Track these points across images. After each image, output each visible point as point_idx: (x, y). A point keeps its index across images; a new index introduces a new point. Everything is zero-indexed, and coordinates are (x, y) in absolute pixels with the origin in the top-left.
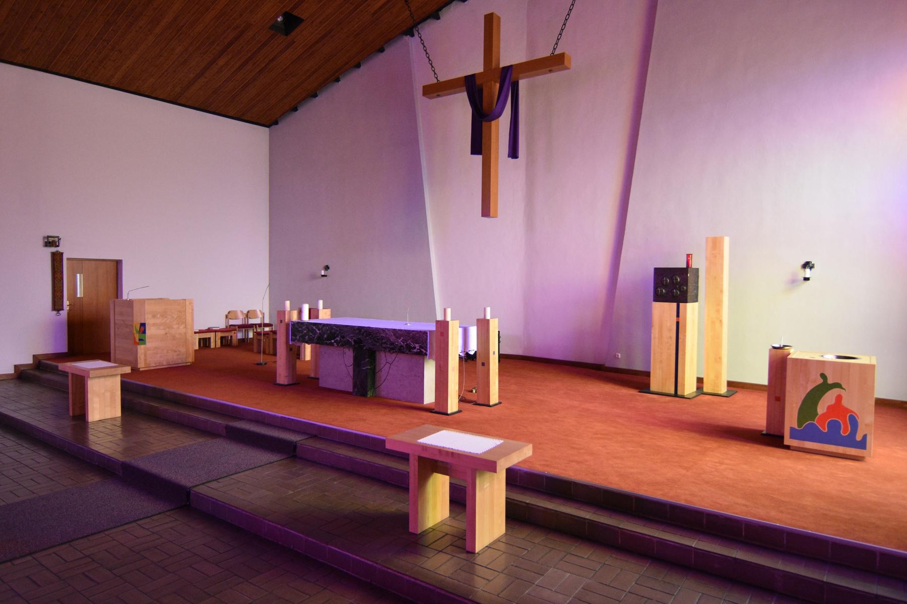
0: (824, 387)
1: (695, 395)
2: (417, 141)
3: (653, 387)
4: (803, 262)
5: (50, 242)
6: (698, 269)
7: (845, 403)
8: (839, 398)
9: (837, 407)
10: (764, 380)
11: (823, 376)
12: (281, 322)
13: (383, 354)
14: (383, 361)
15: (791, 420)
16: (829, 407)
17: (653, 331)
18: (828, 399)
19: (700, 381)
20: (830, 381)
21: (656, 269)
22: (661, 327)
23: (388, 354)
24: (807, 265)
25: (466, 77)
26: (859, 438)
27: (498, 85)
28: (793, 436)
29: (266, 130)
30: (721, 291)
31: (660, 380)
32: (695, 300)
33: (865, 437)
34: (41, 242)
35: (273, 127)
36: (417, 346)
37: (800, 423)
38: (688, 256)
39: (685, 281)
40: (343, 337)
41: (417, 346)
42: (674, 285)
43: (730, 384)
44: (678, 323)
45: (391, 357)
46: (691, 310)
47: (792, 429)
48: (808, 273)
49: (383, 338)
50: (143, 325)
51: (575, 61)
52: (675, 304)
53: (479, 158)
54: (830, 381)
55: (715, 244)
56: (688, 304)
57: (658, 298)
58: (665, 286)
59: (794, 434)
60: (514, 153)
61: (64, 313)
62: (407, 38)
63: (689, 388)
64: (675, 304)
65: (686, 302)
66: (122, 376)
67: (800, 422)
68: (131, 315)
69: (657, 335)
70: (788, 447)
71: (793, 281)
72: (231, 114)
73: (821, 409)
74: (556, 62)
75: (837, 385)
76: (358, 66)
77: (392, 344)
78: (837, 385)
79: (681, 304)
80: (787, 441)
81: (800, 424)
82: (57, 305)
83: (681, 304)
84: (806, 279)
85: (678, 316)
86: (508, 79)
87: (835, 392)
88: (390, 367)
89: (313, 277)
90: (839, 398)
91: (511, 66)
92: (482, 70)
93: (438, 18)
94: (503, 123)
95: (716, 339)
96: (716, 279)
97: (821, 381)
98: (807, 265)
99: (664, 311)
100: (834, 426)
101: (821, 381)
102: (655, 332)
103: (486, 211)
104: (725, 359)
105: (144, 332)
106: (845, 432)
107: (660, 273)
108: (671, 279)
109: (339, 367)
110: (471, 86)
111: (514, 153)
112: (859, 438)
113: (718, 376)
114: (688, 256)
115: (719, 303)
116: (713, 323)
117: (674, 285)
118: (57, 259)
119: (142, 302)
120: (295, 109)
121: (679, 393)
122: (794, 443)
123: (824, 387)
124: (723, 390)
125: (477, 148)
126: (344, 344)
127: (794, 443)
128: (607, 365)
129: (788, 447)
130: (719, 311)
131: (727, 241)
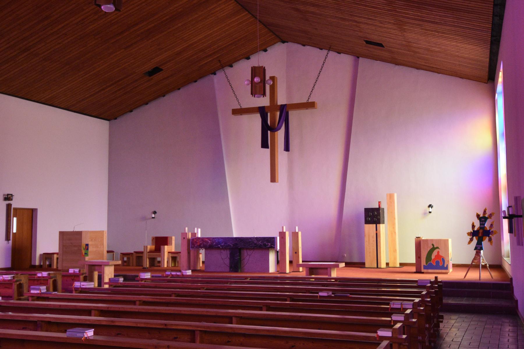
0: (434, 249)
2: (220, 135)
5: (8, 198)
7: (440, 254)
8: (438, 252)
9: (438, 256)
10: (414, 261)
11: (433, 245)
12: (184, 238)
13: (245, 251)
14: (246, 254)
15: (423, 262)
18: (435, 253)
19: (387, 264)
20: (435, 247)
21: (365, 209)
22: (369, 236)
23: (248, 251)
24: (430, 206)
25: (259, 107)
26: (445, 266)
27: (278, 113)
28: (424, 269)
29: (106, 123)
30: (395, 219)
31: (369, 261)
32: (383, 223)
33: (471, 240)
34: (2, 198)
35: (113, 121)
36: (269, 244)
39: (379, 214)
40: (226, 243)
41: (269, 244)
42: (374, 216)
43: (401, 264)
44: (377, 234)
45: (250, 252)
46: (382, 227)
47: (424, 266)
49: (250, 242)
50: (87, 245)
51: (319, 104)
52: (375, 225)
53: (267, 151)
54: (435, 247)
55: (391, 197)
57: (367, 222)
58: (370, 217)
59: (425, 267)
60: (287, 148)
61: (11, 242)
62: (212, 76)
63: (383, 265)
64: (375, 225)
65: (379, 223)
66: (115, 265)
67: (427, 262)
68: (81, 239)
71: (425, 214)
72: (63, 107)
74: (310, 105)
75: (437, 248)
76: (179, 89)
77: (256, 244)
78: (437, 248)
79: (378, 225)
81: (426, 264)
82: (7, 238)
83: (378, 225)
84: (430, 212)
85: (376, 230)
86: (284, 110)
88: (249, 257)
89: (144, 219)
90: (438, 252)
91: (286, 105)
92: (269, 105)
93: (231, 66)
94: (280, 134)
95: (394, 241)
96: (392, 213)
98: (430, 206)
99: (370, 228)
100: (437, 263)
102: (366, 239)
103: (273, 179)
104: (398, 251)
105: (88, 249)
107: (367, 210)
109: (223, 257)
110: (262, 111)
111: (287, 148)
112: (445, 266)
113: (395, 259)
114: (379, 202)
115: (394, 224)
116: (392, 233)
117: (374, 216)
118: (9, 206)
119: (87, 232)
120: (131, 111)
121: (379, 267)
122: (425, 271)
123: (434, 249)
124: (398, 266)
125: (264, 145)
126: (225, 248)
127: (425, 271)
129: (423, 273)
130: (394, 228)
131: (396, 195)
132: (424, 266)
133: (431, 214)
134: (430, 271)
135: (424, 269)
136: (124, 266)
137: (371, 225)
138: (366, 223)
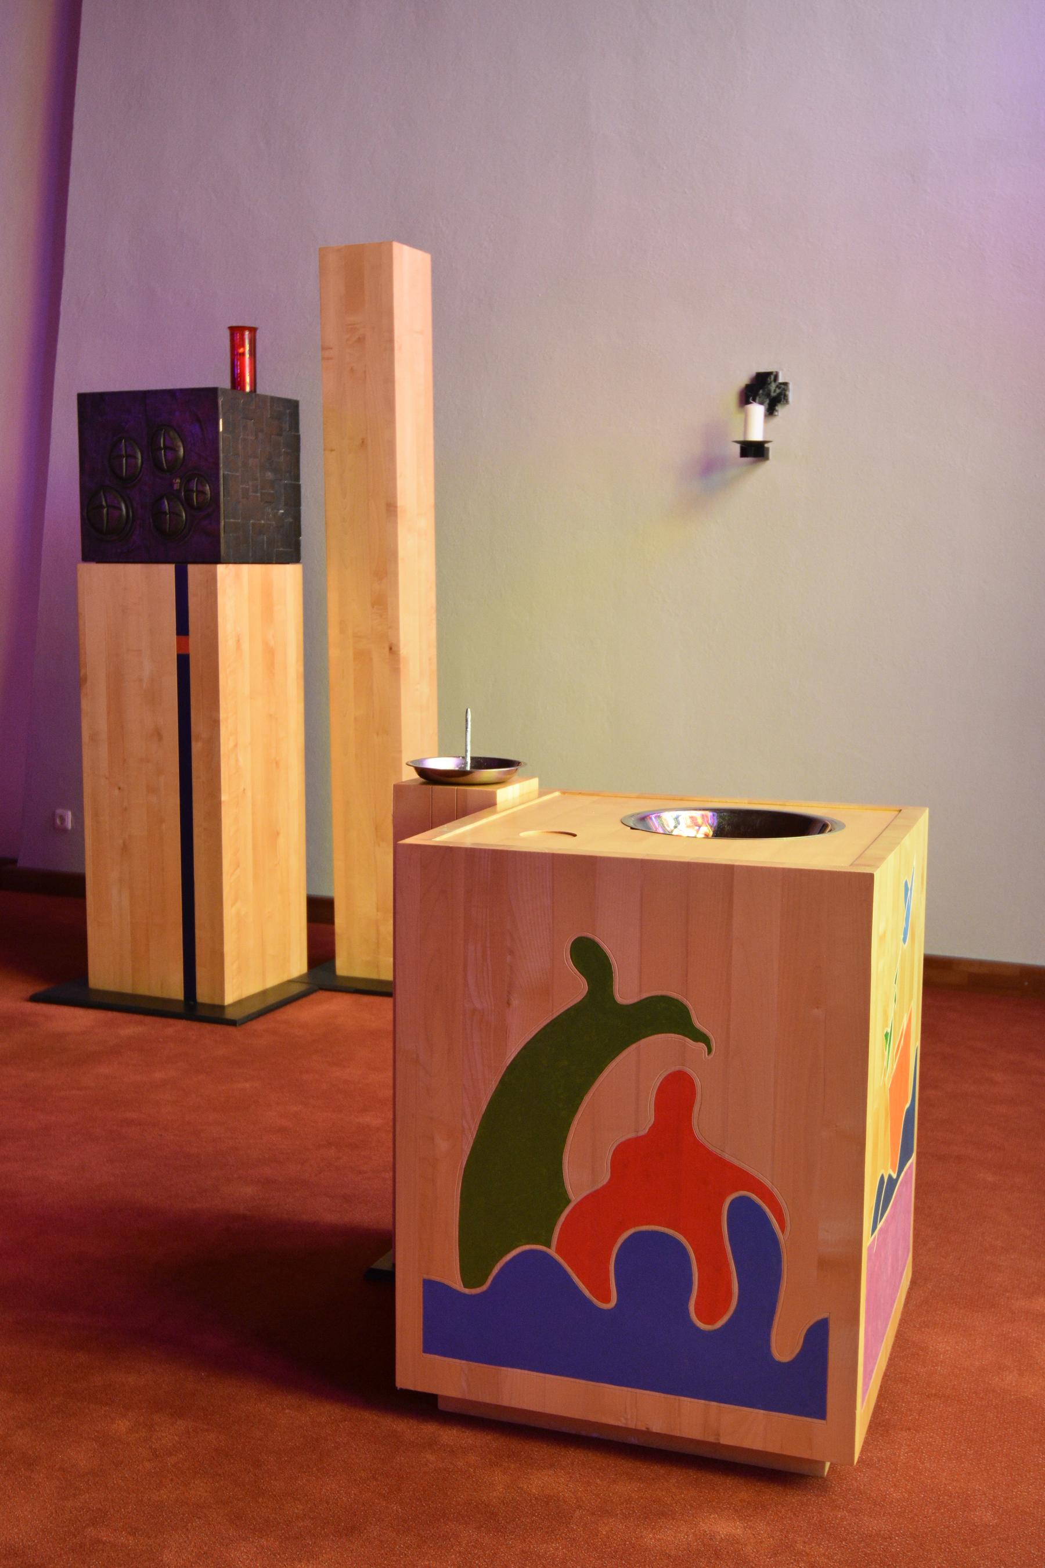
0: (598, 1026)
1: (297, 989)
3: (104, 970)
4: (743, 379)
6: (292, 407)
7: (707, 1124)
8: (677, 1094)
9: (670, 1139)
11: (590, 957)
16: (626, 1156)
17: (85, 704)
18: (618, 1104)
20: (627, 990)
26: (785, 1344)
28: (436, 1341)
31: (123, 940)
33: (818, 1336)
37: (474, 1258)
38: (236, 333)
44: (183, 663)
47: (434, 1292)
48: (756, 423)
52: (167, 572)
54: (627, 990)
56: (221, 569)
57: (103, 542)
59: (453, 1326)
64: (167, 572)
65: (215, 558)
69: (103, 725)
70: (424, 1406)
71: (708, 467)
73: (584, 1168)
75: (666, 1015)
78: (666, 1015)
79: (193, 569)
80: (416, 1367)
81: (473, 1265)
83: (193, 569)
84: (754, 451)
85: (183, 627)
87: (651, 1057)
90: (677, 1094)
97: (575, 988)
98: (765, 390)
99: (120, 601)
100: (653, 1268)
101: (575, 988)
106: (709, 1313)
108: (151, 450)
112: (785, 1344)
121: (203, 995)
123: (598, 1026)
128: (24, 863)
131: (410, 271)
132: (434, 1292)
133: (764, 470)
134: (528, 1390)
135: (436, 1341)
136: (323, 253)
137: (133, 572)
138: (87, 557)
